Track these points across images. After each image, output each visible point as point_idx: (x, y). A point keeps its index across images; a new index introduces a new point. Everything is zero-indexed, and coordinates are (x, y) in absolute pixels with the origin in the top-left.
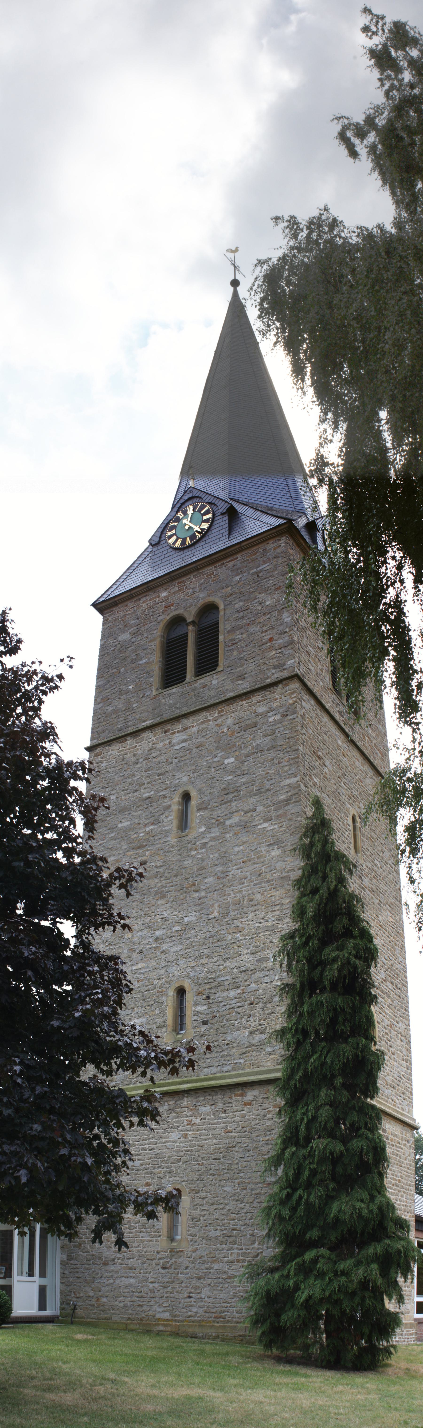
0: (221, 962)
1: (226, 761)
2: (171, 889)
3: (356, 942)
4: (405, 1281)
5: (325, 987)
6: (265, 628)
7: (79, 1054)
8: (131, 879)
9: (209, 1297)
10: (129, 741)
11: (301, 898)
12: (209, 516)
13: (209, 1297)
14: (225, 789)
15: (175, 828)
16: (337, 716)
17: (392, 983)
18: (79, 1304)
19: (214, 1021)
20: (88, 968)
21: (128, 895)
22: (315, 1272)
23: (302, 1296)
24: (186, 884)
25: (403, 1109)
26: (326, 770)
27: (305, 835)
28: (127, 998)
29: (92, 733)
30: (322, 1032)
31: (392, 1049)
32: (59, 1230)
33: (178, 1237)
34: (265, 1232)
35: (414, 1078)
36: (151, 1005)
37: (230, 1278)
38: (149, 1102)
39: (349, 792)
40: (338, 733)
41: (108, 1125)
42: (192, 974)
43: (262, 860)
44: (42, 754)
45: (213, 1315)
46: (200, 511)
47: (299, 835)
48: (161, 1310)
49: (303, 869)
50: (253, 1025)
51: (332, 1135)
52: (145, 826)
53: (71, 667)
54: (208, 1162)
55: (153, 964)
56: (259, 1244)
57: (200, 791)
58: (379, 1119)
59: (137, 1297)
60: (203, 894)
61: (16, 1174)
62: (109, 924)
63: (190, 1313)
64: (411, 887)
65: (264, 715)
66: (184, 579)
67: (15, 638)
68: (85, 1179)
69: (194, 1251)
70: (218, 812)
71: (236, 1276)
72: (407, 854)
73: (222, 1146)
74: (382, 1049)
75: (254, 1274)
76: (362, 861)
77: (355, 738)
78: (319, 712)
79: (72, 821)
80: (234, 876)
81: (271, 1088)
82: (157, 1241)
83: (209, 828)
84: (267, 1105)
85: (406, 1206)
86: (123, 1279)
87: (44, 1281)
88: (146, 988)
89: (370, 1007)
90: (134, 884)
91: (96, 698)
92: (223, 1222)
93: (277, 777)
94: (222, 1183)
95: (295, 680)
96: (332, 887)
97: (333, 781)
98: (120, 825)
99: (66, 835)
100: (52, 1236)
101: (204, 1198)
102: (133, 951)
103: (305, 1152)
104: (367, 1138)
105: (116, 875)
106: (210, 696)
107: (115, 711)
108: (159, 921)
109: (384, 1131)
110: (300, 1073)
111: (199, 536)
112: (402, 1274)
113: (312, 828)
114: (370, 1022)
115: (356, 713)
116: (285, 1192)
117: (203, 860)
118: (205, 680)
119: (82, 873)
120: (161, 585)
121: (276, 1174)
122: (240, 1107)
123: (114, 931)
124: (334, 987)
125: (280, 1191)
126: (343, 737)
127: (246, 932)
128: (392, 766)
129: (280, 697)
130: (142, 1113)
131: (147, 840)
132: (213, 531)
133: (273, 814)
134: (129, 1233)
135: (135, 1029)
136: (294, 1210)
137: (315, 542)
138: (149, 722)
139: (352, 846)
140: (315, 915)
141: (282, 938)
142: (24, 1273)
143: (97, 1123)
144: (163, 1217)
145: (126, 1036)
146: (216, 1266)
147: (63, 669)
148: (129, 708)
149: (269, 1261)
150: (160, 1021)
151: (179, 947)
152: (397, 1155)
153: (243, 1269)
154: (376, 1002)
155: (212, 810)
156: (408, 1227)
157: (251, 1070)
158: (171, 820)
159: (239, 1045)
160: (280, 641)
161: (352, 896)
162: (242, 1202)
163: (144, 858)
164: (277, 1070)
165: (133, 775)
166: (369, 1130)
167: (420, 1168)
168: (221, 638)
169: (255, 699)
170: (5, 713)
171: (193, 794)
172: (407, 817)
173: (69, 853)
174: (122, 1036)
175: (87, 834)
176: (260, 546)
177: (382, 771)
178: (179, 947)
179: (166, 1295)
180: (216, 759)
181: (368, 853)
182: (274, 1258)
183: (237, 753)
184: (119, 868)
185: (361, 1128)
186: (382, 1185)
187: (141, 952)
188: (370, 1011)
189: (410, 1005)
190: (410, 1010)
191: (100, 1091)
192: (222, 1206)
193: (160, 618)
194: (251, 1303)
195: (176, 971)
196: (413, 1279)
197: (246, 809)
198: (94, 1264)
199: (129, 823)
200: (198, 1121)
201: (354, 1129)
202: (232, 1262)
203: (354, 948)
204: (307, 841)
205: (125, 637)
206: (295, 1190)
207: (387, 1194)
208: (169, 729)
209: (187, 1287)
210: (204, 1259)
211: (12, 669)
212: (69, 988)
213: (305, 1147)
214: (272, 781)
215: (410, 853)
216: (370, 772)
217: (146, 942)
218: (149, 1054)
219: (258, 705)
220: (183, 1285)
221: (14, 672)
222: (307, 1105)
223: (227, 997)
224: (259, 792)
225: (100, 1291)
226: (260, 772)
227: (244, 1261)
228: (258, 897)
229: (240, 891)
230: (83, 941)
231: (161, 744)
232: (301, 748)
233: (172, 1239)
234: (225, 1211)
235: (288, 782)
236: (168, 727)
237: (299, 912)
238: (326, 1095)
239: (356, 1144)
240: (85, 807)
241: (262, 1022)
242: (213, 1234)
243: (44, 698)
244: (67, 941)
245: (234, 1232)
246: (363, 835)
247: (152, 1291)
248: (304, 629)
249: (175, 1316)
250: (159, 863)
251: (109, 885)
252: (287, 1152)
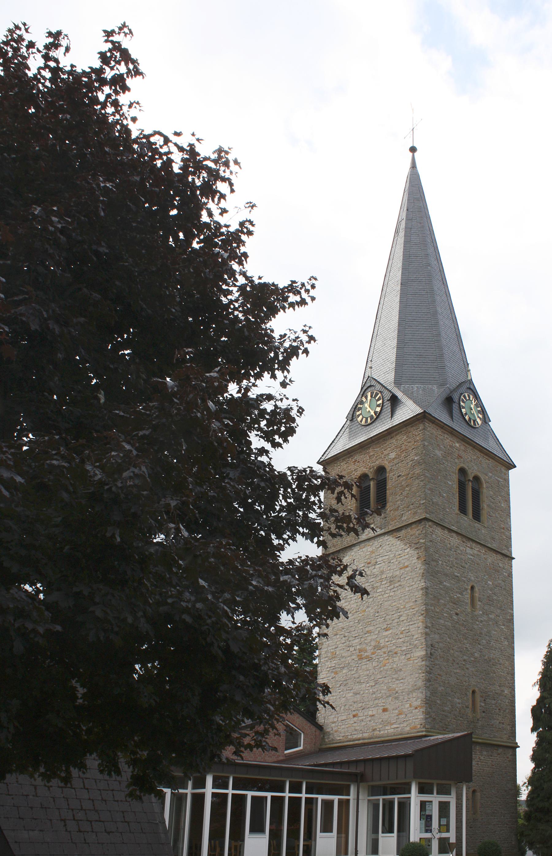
132: (383, 414)
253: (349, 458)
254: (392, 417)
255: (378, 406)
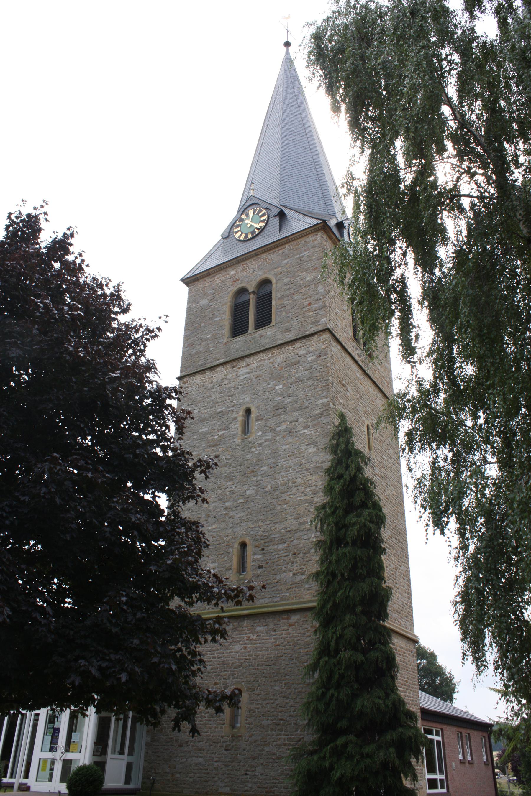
0: (272, 525)
1: (277, 387)
2: (237, 474)
3: (370, 511)
4: (417, 762)
5: (348, 543)
6: (305, 296)
7: (169, 590)
8: (209, 467)
9: (261, 775)
10: (208, 373)
11: (330, 481)
12: (265, 217)
13: (261, 775)
14: (276, 406)
15: (240, 433)
16: (356, 357)
17: (396, 539)
18: (158, 778)
19: (267, 566)
20: (178, 530)
21: (207, 478)
22: (346, 755)
23: (336, 775)
24: (247, 471)
25: (406, 628)
26: (348, 394)
27: (333, 438)
28: (205, 551)
29: (181, 367)
30: (346, 574)
31: (397, 585)
32: (147, 720)
33: (238, 725)
34: (306, 722)
35: (414, 605)
36: (222, 554)
37: (278, 758)
38: (220, 624)
39: (364, 409)
40: (357, 369)
41: (189, 641)
42: (252, 533)
43: (302, 455)
44: (147, 382)
45: (265, 790)
46: (258, 214)
47: (329, 438)
48: (223, 785)
49: (332, 461)
50: (295, 569)
51: (355, 649)
52: (219, 431)
53: (166, 322)
54: (262, 668)
55: (223, 525)
56: (301, 731)
57: (258, 407)
58: (389, 636)
59: (204, 773)
60: (259, 478)
61: (118, 676)
62: (193, 497)
63: (246, 788)
64: (410, 474)
65: (304, 356)
66: (247, 262)
67: (126, 303)
68: (170, 681)
69: (251, 736)
70: (271, 422)
71: (282, 757)
72: (407, 451)
73: (272, 656)
74: (390, 585)
75: (297, 757)
76: (374, 456)
77: (369, 372)
78: (344, 354)
79: (168, 427)
80: (282, 466)
81: (309, 614)
82: (222, 728)
83: (264, 433)
84: (306, 626)
85: (413, 700)
86: (194, 758)
87: (131, 759)
88: (218, 542)
89: (380, 556)
90: (211, 471)
91: (184, 344)
92: (273, 714)
93: (313, 398)
94: (272, 684)
95: (327, 332)
96: (353, 474)
97: (353, 402)
98: (200, 431)
99: (163, 437)
100: (141, 724)
101: (258, 695)
102: (209, 516)
103: (335, 661)
104: (381, 650)
105: (198, 464)
106: (265, 343)
107: (198, 353)
108: (228, 493)
109: (394, 644)
110: (331, 604)
111: (257, 231)
112: (414, 756)
113: (338, 433)
114: (381, 567)
115: (370, 356)
116: (320, 691)
117: (260, 454)
118: (262, 331)
119: (174, 463)
120: (230, 266)
121: (313, 677)
122: (286, 628)
123: (196, 504)
124: (354, 543)
125: (317, 690)
126: (360, 371)
127: (291, 504)
128: (396, 391)
129: (315, 344)
130: (214, 632)
131: (220, 441)
133: (310, 423)
134: (201, 721)
135: (210, 572)
136: (328, 705)
137: (342, 235)
138: (222, 361)
139: (367, 446)
140: (340, 491)
141: (317, 509)
142: (116, 752)
143: (181, 639)
144: (227, 709)
145: (204, 577)
146: (267, 749)
147: (160, 323)
148: (207, 351)
149: (310, 745)
150: (228, 565)
151: (242, 514)
152: (404, 662)
153: (288, 752)
154: (385, 553)
155: (267, 420)
156: (416, 717)
157: (294, 601)
158: (237, 427)
159: (285, 583)
160: (316, 305)
161: (367, 480)
162: (288, 698)
163: (217, 453)
164: (314, 601)
165: (210, 396)
166: (382, 644)
167: (421, 670)
168: (274, 303)
169: (298, 344)
170: (120, 353)
171: (253, 409)
172: (406, 426)
173: (164, 449)
174: (201, 577)
175: (178, 436)
176: (302, 239)
177: (388, 395)
178: (242, 514)
179: (227, 772)
180: (269, 386)
181: (378, 451)
182: (312, 743)
183: (285, 382)
184: (200, 459)
185: (376, 643)
186: (394, 686)
187: (215, 517)
188: (380, 559)
189: (409, 554)
190: (409, 557)
191: (184, 616)
192: (272, 701)
193: (229, 289)
194: (295, 780)
195: (240, 531)
196: (423, 760)
197: (291, 420)
198: (172, 745)
199: (207, 429)
200: (255, 637)
201: (372, 644)
202: (280, 746)
203: (369, 515)
204: (334, 442)
205: (204, 302)
206: (328, 689)
207: (399, 692)
208: (236, 366)
209: (244, 766)
210: (257, 743)
211: (125, 323)
212: (163, 543)
213: (335, 656)
214: (310, 401)
215: (409, 450)
216: (380, 395)
217: (218, 510)
218: (220, 591)
219: (300, 349)
220: (241, 764)
221: (127, 326)
222: (336, 626)
223: (277, 549)
224: (300, 408)
225: (175, 768)
226: (301, 395)
227: (289, 745)
228: (299, 480)
229: (287, 477)
230: (174, 511)
231: (231, 375)
232: (330, 379)
233: (233, 726)
234: (274, 705)
235: (321, 401)
236: (235, 364)
237: (329, 489)
238: (350, 619)
239: (373, 655)
240: (177, 417)
241: (302, 567)
242: (265, 722)
243: (147, 343)
244: (163, 511)
245: (282, 722)
246: (375, 438)
247: (216, 769)
248: (333, 297)
249: (235, 790)
250: (228, 457)
251: (193, 471)
252: (322, 661)
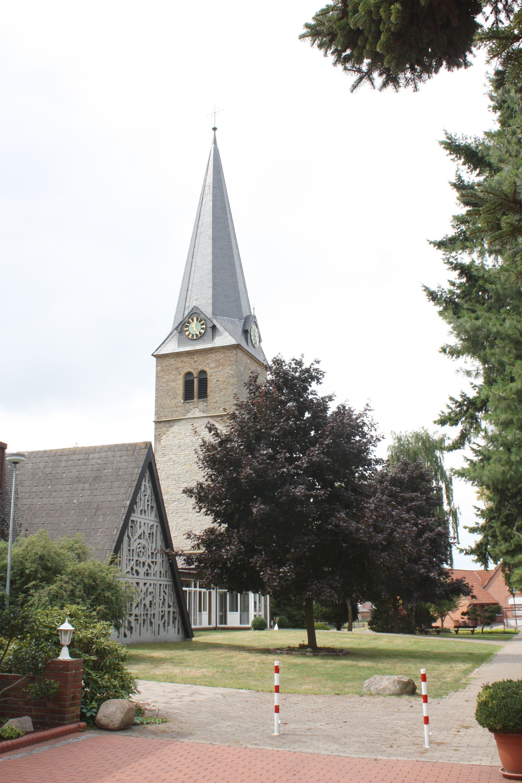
253: (177, 357)
254: (213, 339)
255: (203, 329)
